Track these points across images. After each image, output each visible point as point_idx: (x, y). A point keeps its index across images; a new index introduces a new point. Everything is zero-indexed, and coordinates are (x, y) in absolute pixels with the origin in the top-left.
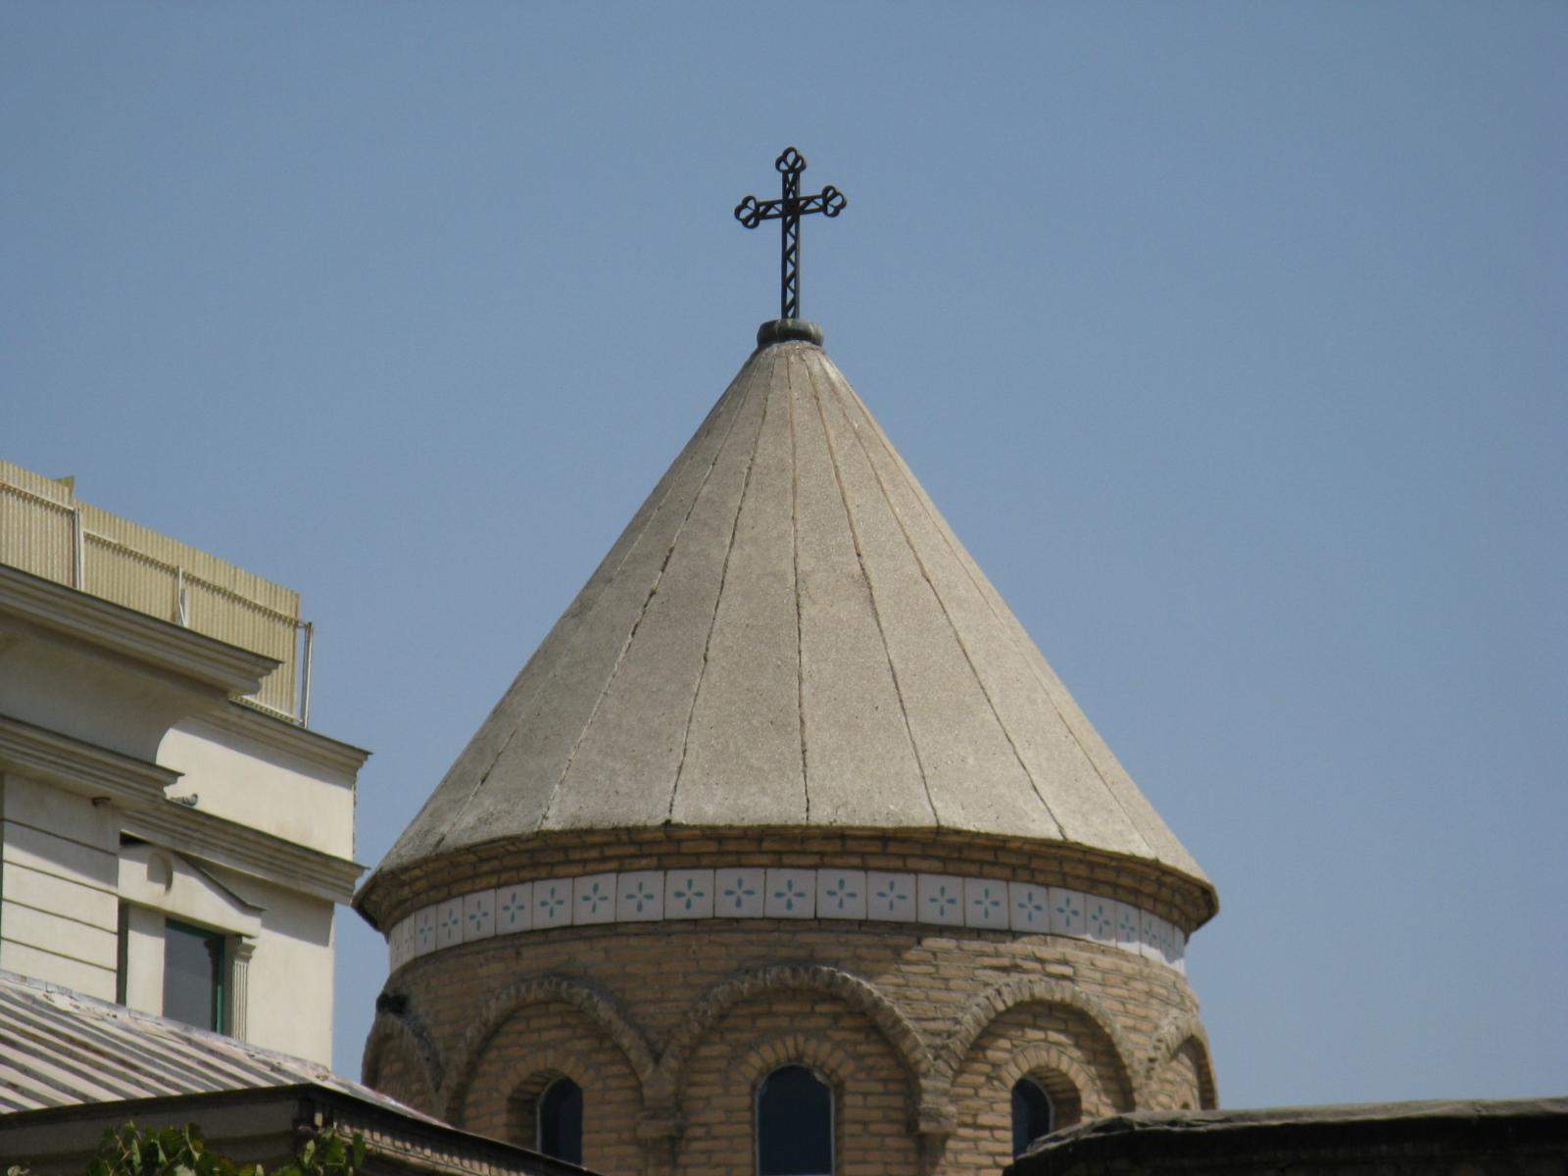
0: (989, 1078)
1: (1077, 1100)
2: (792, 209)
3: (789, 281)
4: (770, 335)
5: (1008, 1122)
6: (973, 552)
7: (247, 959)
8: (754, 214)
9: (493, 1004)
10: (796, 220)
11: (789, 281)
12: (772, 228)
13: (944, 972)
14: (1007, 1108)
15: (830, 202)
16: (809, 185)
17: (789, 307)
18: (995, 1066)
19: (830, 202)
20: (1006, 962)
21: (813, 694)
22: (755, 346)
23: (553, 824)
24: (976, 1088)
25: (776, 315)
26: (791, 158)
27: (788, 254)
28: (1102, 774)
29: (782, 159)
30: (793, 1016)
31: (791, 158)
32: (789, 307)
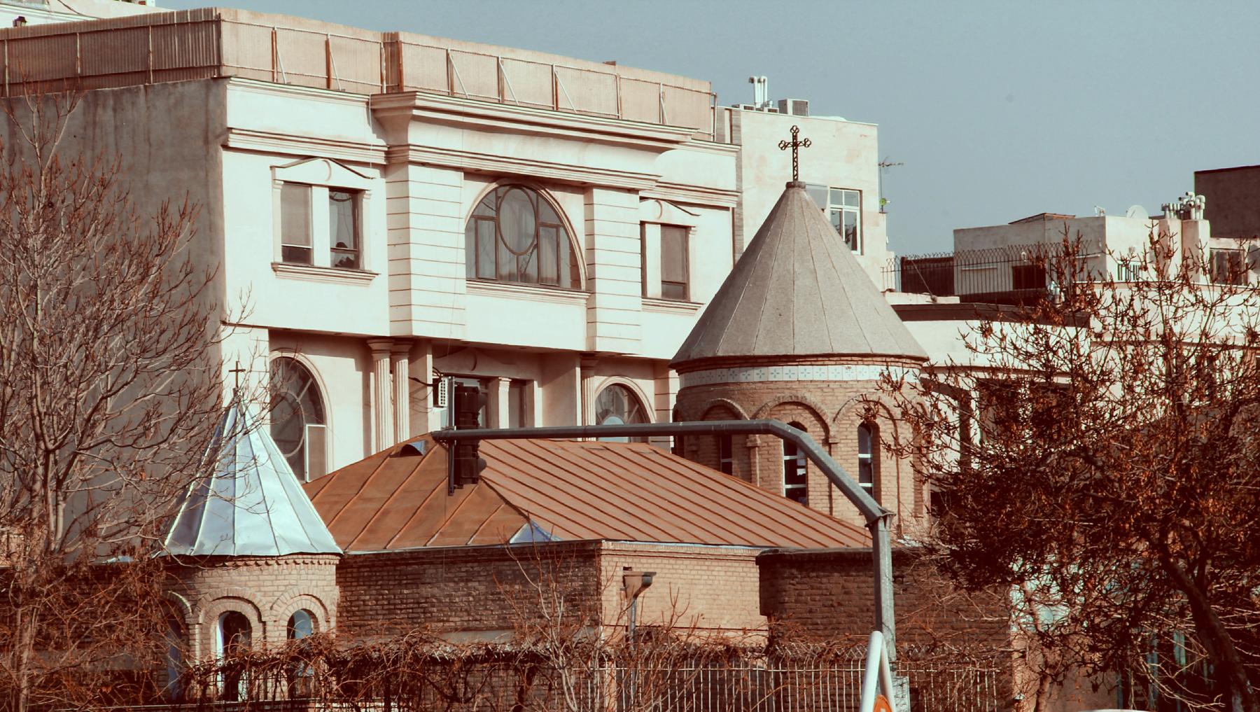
0: (851, 424)
1: (862, 425)
2: (795, 145)
3: (795, 168)
4: (789, 186)
5: (857, 437)
6: (295, 474)
7: (643, 442)
8: (784, 146)
9: (889, 505)
10: (796, 148)
11: (795, 168)
12: (790, 150)
13: (837, 394)
14: (856, 433)
15: (806, 143)
16: (800, 138)
17: (795, 176)
18: (852, 421)
19: (806, 143)
20: (855, 390)
21: (143, 470)
22: (785, 189)
23: (720, 354)
24: (847, 428)
25: (791, 180)
26: (795, 128)
27: (795, 160)
28: (78, 412)
29: (792, 129)
30: (791, 410)
31: (795, 128)
32: (795, 176)
